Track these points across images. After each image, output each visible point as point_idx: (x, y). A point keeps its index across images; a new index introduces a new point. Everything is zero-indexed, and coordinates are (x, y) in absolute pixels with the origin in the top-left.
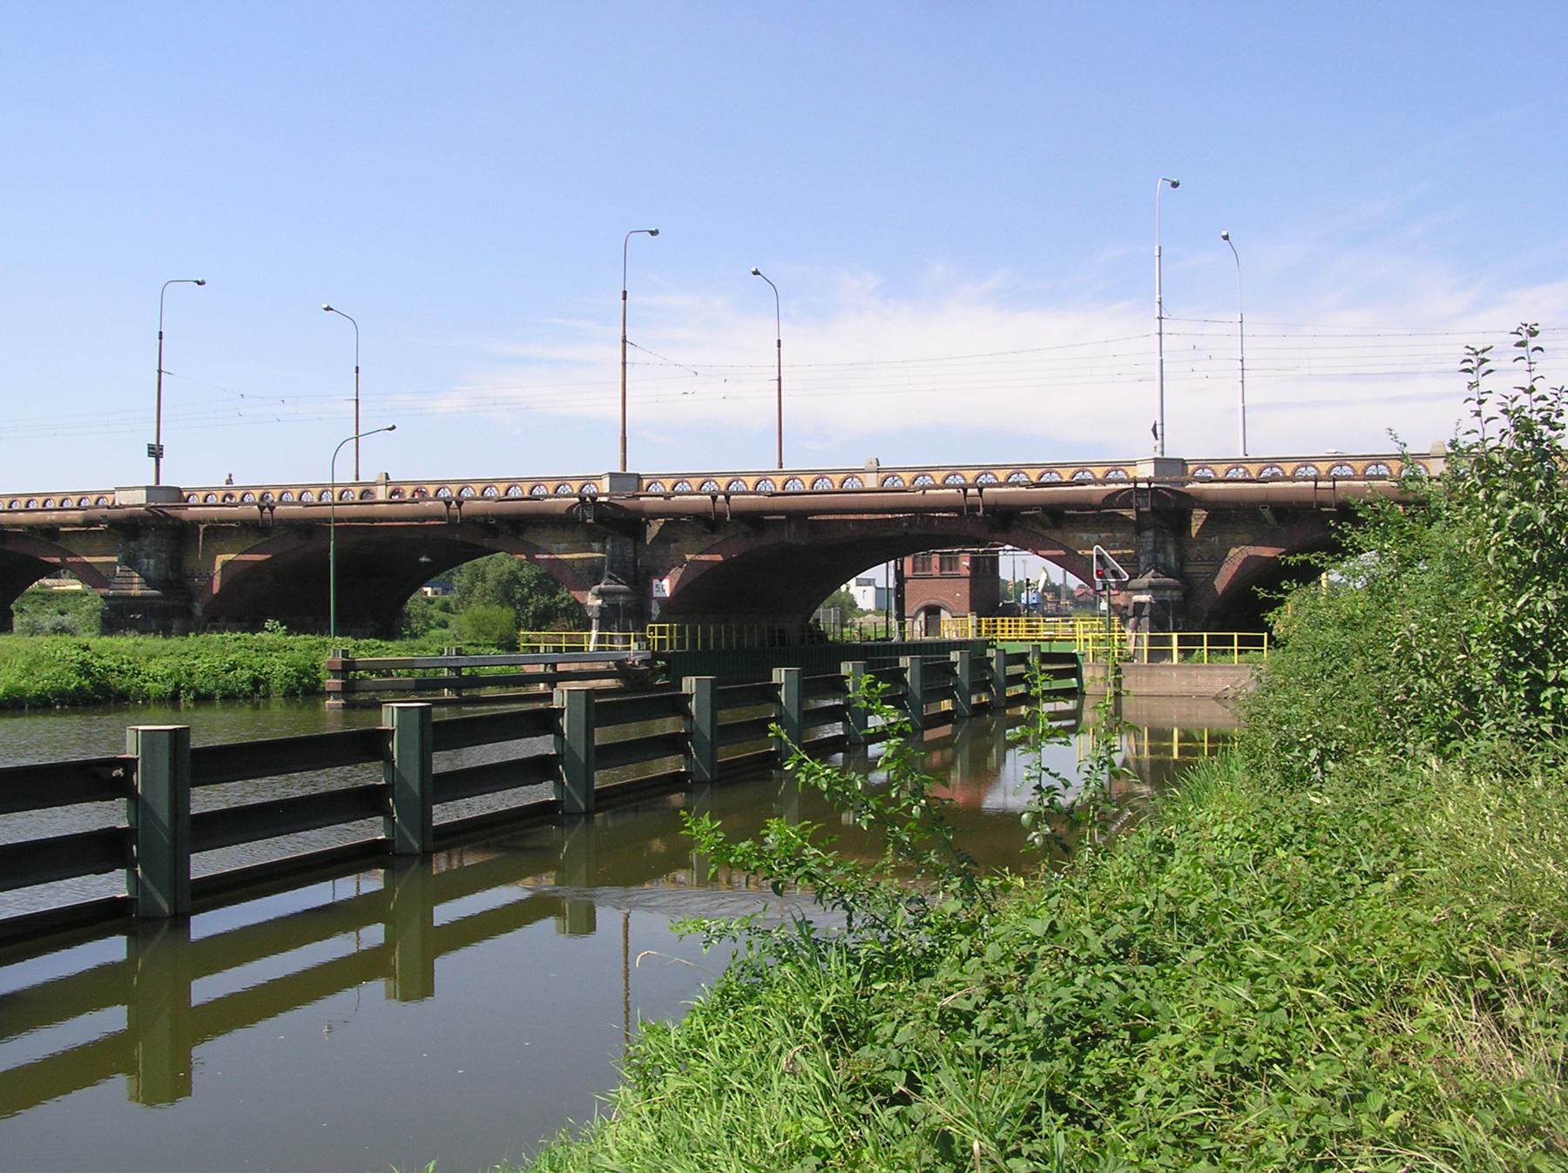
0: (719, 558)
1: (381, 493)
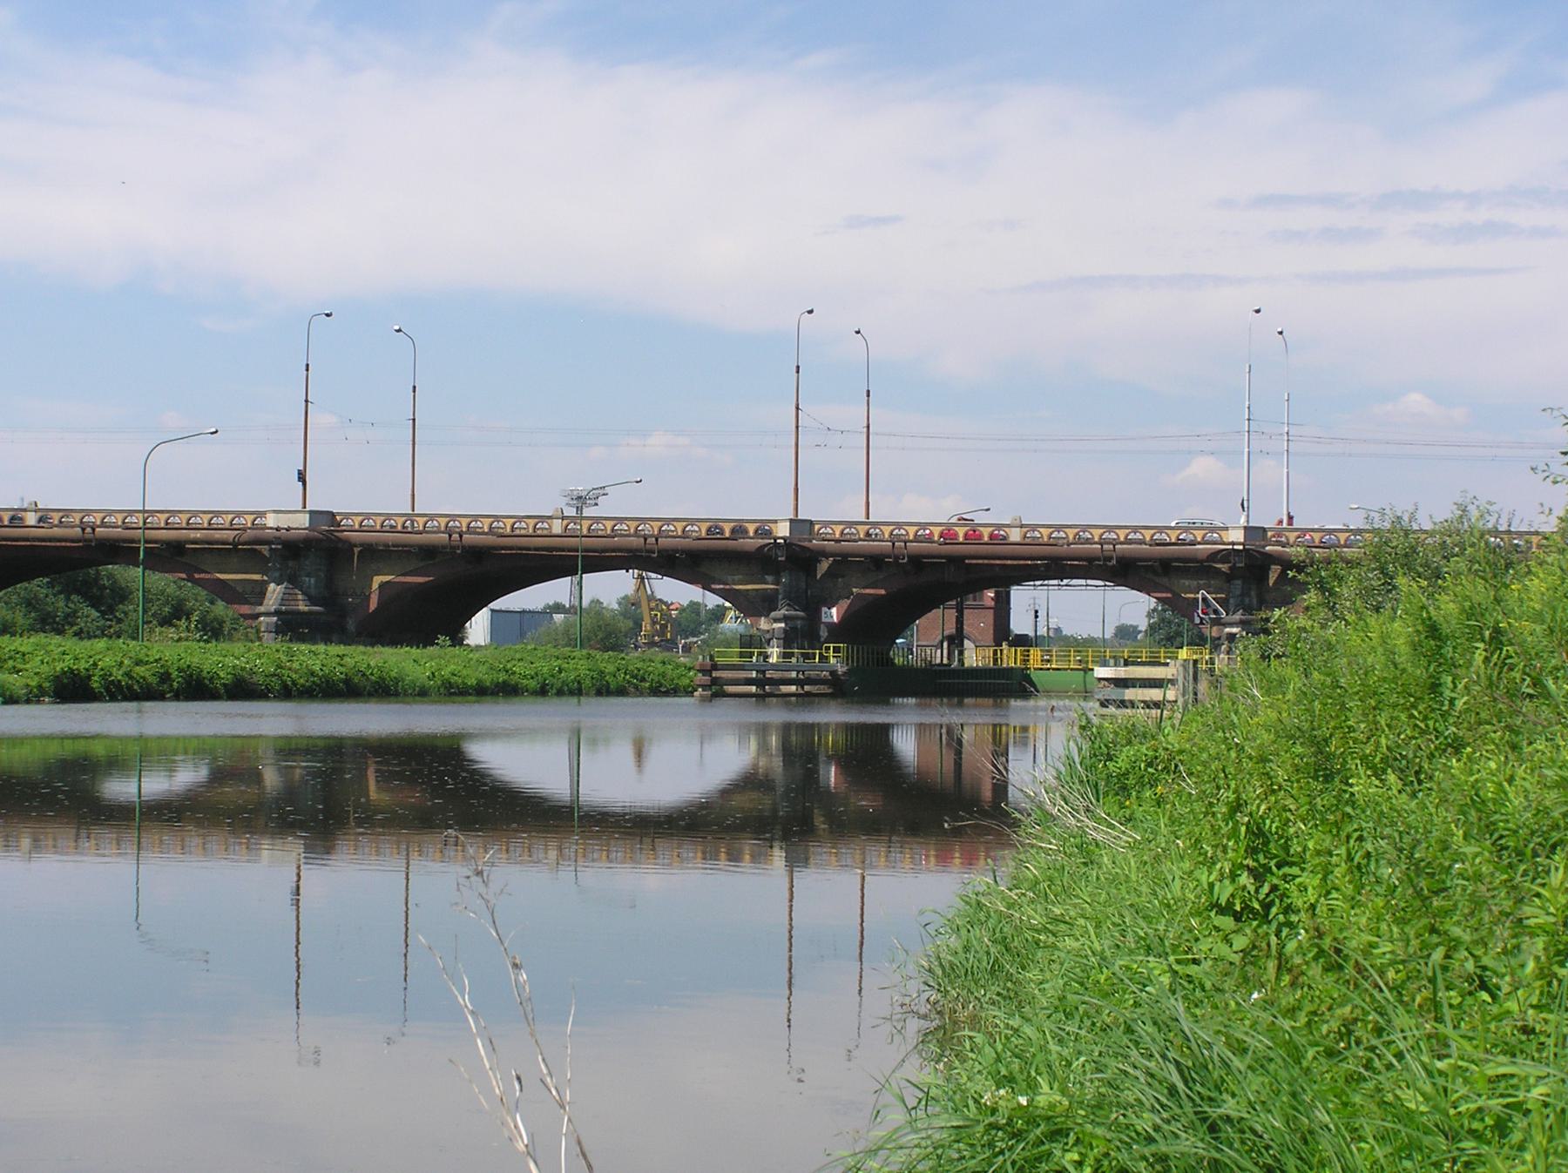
0: (883, 592)
1: (31, 519)
